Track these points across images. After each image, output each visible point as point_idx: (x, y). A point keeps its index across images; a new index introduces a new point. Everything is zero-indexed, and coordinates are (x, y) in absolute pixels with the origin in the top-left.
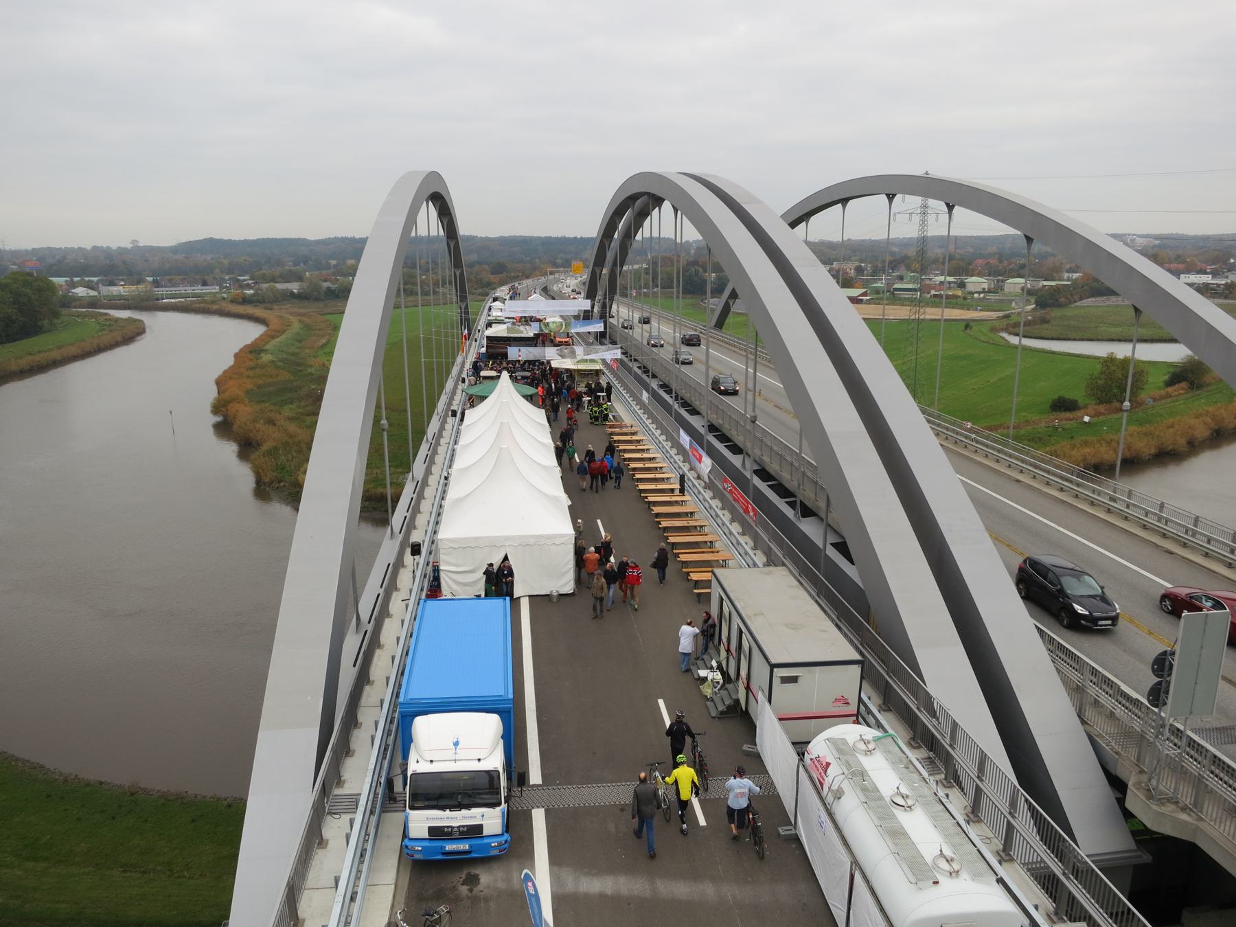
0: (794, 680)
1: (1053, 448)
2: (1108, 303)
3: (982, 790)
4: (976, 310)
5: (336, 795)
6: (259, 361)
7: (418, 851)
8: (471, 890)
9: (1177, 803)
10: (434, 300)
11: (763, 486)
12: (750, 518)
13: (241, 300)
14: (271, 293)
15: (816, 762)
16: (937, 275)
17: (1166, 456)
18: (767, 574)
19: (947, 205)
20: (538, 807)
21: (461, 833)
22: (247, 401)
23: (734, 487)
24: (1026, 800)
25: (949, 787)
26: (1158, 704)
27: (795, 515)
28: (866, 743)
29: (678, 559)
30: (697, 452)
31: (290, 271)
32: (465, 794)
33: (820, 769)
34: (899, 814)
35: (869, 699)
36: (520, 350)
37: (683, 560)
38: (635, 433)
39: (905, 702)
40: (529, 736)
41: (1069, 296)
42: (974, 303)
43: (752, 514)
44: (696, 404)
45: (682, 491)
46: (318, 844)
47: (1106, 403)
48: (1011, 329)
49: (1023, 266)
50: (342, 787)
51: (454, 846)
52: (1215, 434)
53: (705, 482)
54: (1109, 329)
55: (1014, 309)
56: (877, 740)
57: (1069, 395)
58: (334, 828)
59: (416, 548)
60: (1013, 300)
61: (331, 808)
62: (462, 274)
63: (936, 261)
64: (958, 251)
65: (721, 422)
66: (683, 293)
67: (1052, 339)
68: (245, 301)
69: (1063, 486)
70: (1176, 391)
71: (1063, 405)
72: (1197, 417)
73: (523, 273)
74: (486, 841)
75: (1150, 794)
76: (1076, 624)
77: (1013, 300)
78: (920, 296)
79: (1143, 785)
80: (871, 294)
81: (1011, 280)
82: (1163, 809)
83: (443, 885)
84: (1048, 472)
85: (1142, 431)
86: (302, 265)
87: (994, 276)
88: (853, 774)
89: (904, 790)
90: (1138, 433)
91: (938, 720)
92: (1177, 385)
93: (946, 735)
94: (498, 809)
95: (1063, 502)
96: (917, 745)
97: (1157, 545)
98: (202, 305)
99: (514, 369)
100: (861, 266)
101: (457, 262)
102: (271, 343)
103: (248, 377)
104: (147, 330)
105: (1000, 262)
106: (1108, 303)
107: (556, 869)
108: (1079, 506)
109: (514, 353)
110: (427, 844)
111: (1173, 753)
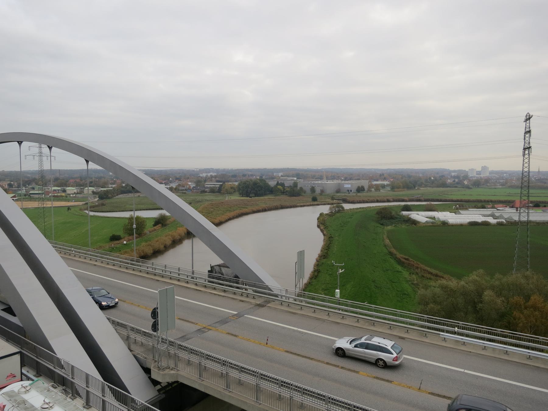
2: (128, 196)
4: (72, 201)
19: (49, 146)
24: (108, 386)
26: (156, 330)
39: (47, 367)
41: (112, 194)
42: (71, 199)
54: (130, 206)
56: (30, 385)
57: (117, 234)
64: (61, 176)
67: (107, 212)
70: (157, 228)
71: (115, 238)
75: (159, 368)
78: (44, 196)
79: (156, 366)
80: (17, 197)
85: (147, 244)
87: (79, 187)
88: (19, 404)
91: (65, 369)
93: (69, 375)
95: (115, 270)
100: (11, 183)
106: (128, 196)
111: (164, 348)
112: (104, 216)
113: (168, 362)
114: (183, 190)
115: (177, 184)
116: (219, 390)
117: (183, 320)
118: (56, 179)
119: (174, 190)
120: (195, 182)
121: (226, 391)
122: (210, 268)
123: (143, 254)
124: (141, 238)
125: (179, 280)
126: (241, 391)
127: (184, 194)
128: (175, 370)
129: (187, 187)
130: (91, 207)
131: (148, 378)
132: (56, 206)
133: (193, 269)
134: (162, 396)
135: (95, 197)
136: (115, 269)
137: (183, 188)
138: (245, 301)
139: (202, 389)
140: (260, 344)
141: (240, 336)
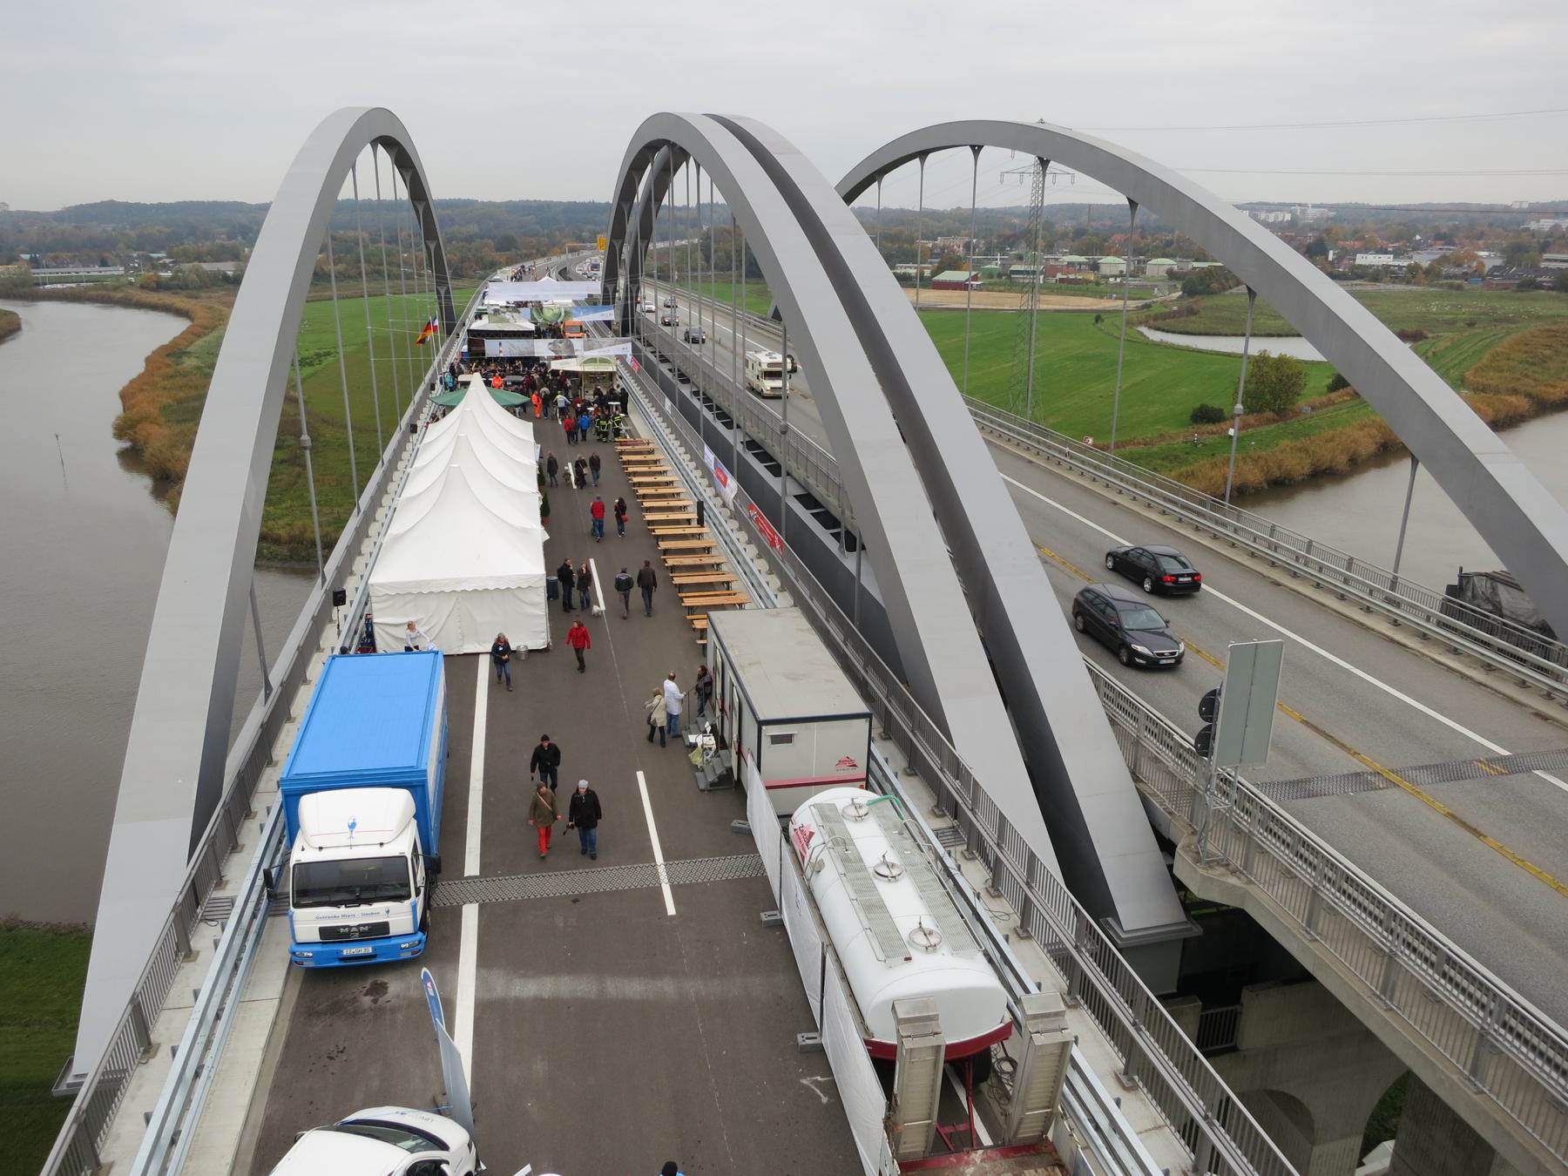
0: (788, 739)
1: (1190, 468)
3: (1001, 862)
4: (1111, 298)
5: (215, 899)
6: (179, 367)
7: (308, 957)
8: (375, 1001)
9: (1228, 865)
10: (418, 285)
11: (805, 515)
12: (776, 552)
13: (155, 286)
14: (195, 276)
15: (799, 833)
16: (1064, 254)
17: (1322, 476)
18: (774, 616)
20: (471, 902)
21: (362, 934)
22: (163, 420)
23: (760, 515)
25: (971, 859)
27: (840, 549)
28: (857, 807)
29: (683, 604)
30: (721, 471)
31: (223, 246)
32: (365, 888)
33: (802, 840)
34: (883, 887)
35: (887, 761)
36: (500, 344)
37: (687, 605)
38: (651, 452)
40: (470, 820)
41: (1223, 281)
42: (1109, 290)
43: (778, 547)
44: (736, 416)
45: (701, 522)
46: (184, 957)
47: (1258, 412)
48: (1151, 322)
49: (1169, 243)
50: (224, 889)
51: (354, 950)
52: (1382, 449)
53: (730, 510)
54: (1269, 322)
55: (1156, 297)
56: (872, 803)
57: (1214, 403)
58: (203, 937)
59: (339, 596)
60: (1156, 286)
61: (206, 914)
62: (438, 247)
63: (1064, 236)
65: (762, 436)
66: (746, 276)
67: (1200, 334)
68: (160, 286)
69: (1165, 509)
70: (1340, 397)
71: (1206, 416)
72: (1361, 429)
73: (538, 250)
74: (394, 942)
76: (1134, 663)
77: (1156, 286)
81: (1154, 261)
82: (1212, 873)
83: (341, 997)
84: (1150, 492)
86: (240, 238)
89: (891, 858)
90: (1291, 449)
92: (1341, 390)
94: (407, 903)
96: (940, 813)
97: (1264, 576)
98: (100, 292)
99: (496, 370)
101: (430, 231)
102: (197, 343)
103: (165, 388)
104: (24, 326)
105: (1143, 238)
107: (484, 972)
108: (1181, 532)
109: (492, 348)
110: (318, 948)
112: (1187, 346)
113: (1226, 845)
114: (1455, 277)
115: (1436, 257)
116: (1358, 990)
117: (1316, 729)
118: (1080, 232)
119: (1423, 276)
120: (1503, 251)
121: (1378, 1001)
122: (1457, 579)
123: (1277, 473)
124: (1281, 424)
125: (1342, 598)
126: (1426, 1020)
127: (1454, 292)
128: (1243, 877)
129: (1469, 267)
130: (1156, 318)
131: (1166, 868)
132: (1070, 308)
133: (1396, 571)
134: (1196, 930)
135: (1173, 289)
136: (1165, 524)
137: (1457, 271)
138: (1555, 720)
139: (1308, 965)
140: (1556, 889)
141: (1491, 839)
